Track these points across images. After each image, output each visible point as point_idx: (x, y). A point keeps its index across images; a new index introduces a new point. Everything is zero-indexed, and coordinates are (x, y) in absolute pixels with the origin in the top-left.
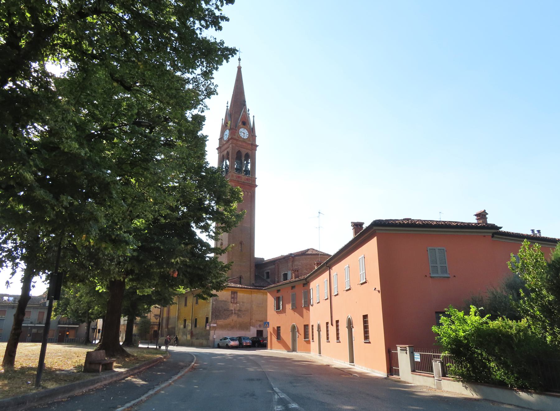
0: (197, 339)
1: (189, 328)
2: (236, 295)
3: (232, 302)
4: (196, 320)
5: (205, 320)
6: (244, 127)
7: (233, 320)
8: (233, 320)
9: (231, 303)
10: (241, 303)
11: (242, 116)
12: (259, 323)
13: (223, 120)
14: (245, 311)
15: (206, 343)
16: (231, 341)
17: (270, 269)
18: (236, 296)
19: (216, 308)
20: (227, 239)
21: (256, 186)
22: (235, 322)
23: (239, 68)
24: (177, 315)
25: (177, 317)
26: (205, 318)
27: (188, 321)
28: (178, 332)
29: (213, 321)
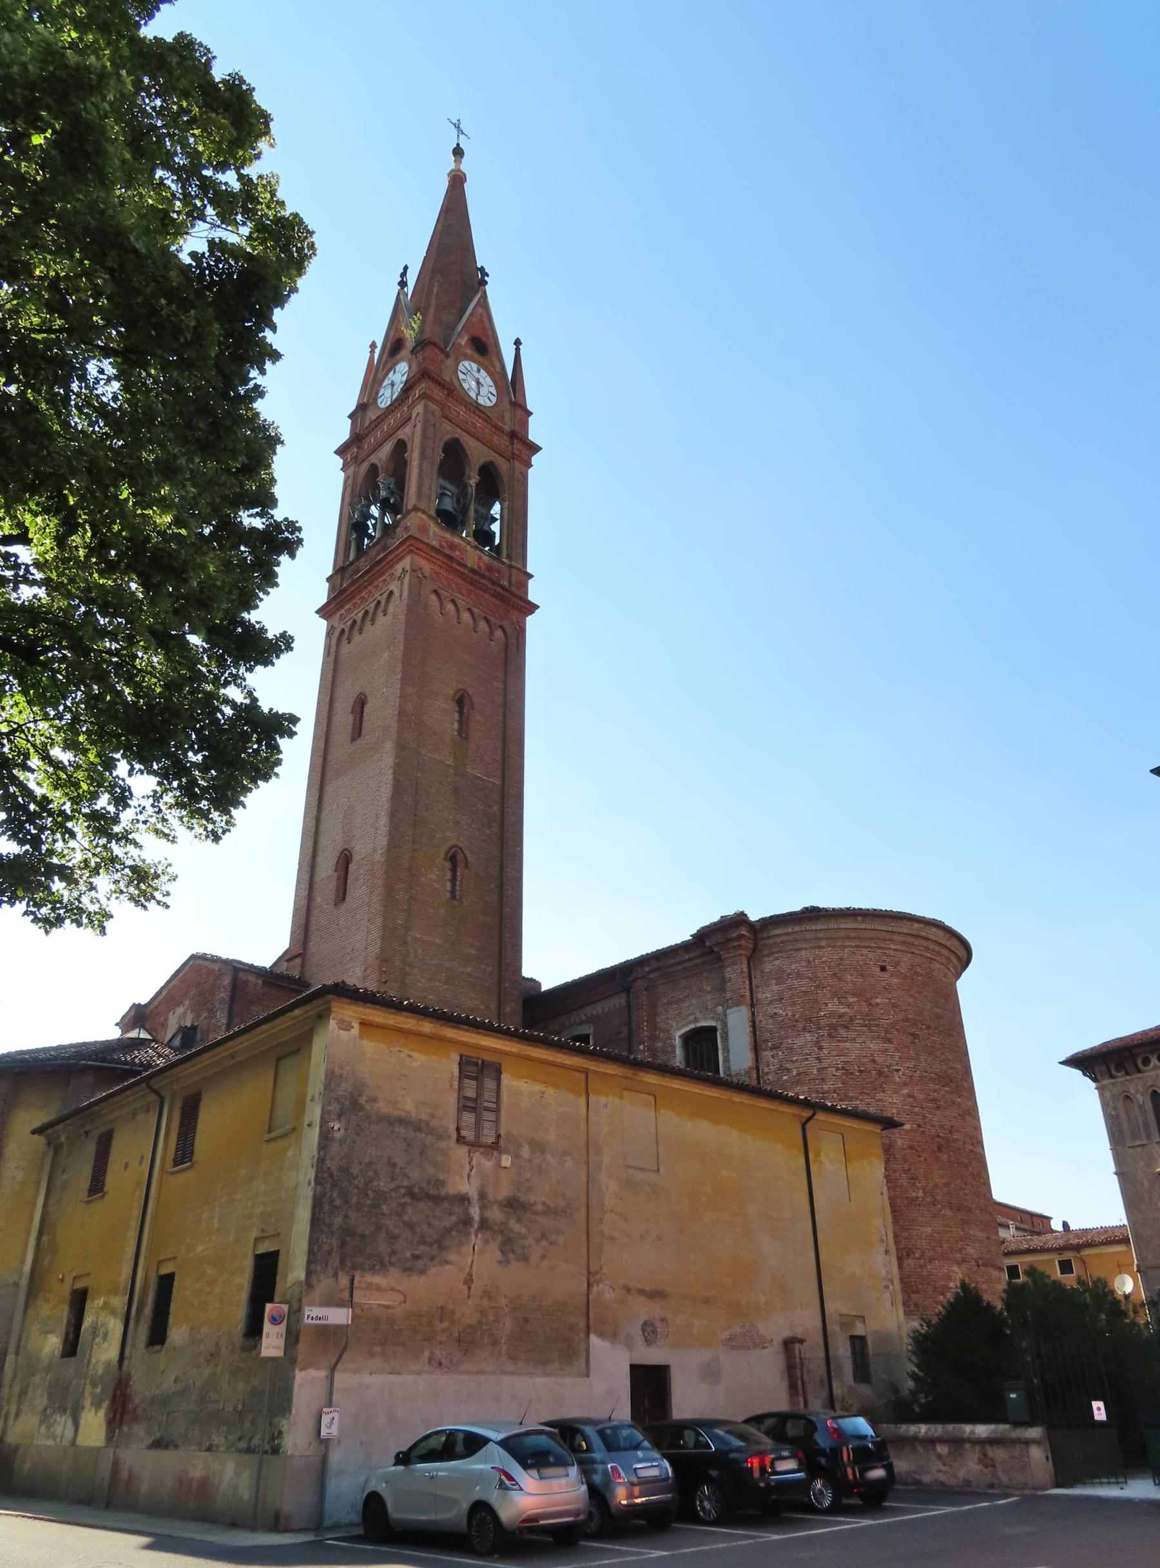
0: (157, 1444)
1: (106, 1352)
2: (489, 1084)
3: (468, 1134)
4: (166, 1284)
5: (243, 1281)
6: (480, 359)
7: (469, 1280)
8: (469, 1280)
9: (460, 1140)
10: (526, 1152)
11: (471, 314)
12: (644, 1310)
13: (373, 346)
14: (548, 1211)
15: (245, 1493)
16: (515, 1469)
17: (590, 1020)
18: (489, 1095)
19: (345, 1170)
20: (384, 821)
21: (532, 608)
22: (486, 1294)
23: (457, 181)
24: (27, 1267)
25: (24, 1282)
26: (249, 1263)
27: (101, 1302)
28: (17, 1389)
29: (325, 1283)
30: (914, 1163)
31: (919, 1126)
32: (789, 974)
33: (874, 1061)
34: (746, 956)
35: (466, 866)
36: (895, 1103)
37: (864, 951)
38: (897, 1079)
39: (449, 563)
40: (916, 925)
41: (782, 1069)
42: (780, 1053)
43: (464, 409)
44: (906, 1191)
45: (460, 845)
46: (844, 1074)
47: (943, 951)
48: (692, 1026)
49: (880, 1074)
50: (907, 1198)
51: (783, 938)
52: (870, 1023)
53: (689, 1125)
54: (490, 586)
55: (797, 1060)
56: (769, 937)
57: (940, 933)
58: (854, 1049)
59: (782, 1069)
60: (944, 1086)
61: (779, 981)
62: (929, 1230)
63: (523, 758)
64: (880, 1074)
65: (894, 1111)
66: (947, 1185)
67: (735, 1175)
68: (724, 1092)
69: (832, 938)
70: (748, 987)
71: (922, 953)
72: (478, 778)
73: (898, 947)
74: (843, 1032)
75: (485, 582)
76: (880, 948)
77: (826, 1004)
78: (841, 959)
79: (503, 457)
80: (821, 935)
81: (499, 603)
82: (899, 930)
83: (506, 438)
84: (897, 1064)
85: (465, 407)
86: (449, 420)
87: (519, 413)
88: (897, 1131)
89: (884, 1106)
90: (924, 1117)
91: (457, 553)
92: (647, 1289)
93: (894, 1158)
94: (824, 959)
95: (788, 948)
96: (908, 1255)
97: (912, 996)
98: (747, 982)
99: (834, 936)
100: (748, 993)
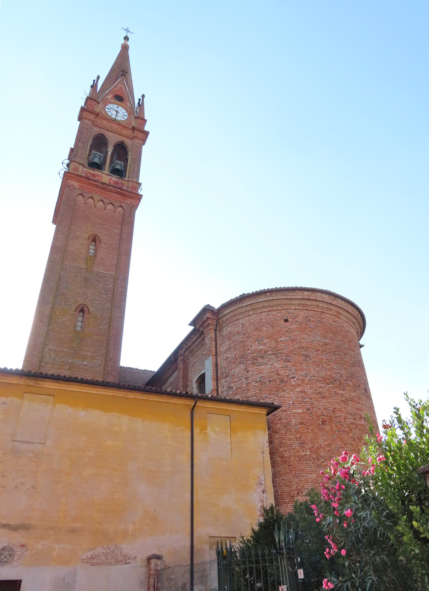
23: (125, 48)
30: (304, 434)
31: (309, 410)
32: (234, 334)
33: (278, 374)
34: (213, 329)
35: (89, 313)
36: (291, 397)
37: (274, 313)
38: (293, 383)
39: (89, 181)
40: (306, 293)
41: (230, 388)
42: (229, 379)
44: (298, 451)
45: (86, 303)
46: (260, 384)
47: (331, 307)
48: (199, 375)
49: (282, 381)
50: (298, 456)
51: (231, 315)
52: (276, 353)
53: (83, 413)
54: (113, 189)
55: (236, 381)
56: (224, 316)
57: (327, 297)
58: (266, 369)
59: (230, 388)
60: (328, 384)
61: (229, 338)
62: (314, 476)
63: (130, 262)
64: (282, 381)
65: (291, 402)
66: (329, 445)
67: (120, 444)
69: (255, 309)
70: (214, 346)
71: (315, 309)
72: (101, 273)
73: (296, 307)
74: (260, 360)
75: (111, 188)
76: (284, 310)
77: (252, 346)
78: (261, 319)
79: (129, 138)
80: (248, 308)
81: (120, 196)
82: (294, 297)
83: (130, 131)
84: (293, 374)
85: (107, 120)
86: (97, 127)
87: (139, 121)
88: (278, 411)
89: (284, 400)
91: (97, 178)
92: (12, 523)
93: (290, 431)
94: (251, 322)
95: (234, 320)
96: (298, 494)
97: (306, 333)
98: (214, 343)
99: (255, 308)
100: (214, 349)
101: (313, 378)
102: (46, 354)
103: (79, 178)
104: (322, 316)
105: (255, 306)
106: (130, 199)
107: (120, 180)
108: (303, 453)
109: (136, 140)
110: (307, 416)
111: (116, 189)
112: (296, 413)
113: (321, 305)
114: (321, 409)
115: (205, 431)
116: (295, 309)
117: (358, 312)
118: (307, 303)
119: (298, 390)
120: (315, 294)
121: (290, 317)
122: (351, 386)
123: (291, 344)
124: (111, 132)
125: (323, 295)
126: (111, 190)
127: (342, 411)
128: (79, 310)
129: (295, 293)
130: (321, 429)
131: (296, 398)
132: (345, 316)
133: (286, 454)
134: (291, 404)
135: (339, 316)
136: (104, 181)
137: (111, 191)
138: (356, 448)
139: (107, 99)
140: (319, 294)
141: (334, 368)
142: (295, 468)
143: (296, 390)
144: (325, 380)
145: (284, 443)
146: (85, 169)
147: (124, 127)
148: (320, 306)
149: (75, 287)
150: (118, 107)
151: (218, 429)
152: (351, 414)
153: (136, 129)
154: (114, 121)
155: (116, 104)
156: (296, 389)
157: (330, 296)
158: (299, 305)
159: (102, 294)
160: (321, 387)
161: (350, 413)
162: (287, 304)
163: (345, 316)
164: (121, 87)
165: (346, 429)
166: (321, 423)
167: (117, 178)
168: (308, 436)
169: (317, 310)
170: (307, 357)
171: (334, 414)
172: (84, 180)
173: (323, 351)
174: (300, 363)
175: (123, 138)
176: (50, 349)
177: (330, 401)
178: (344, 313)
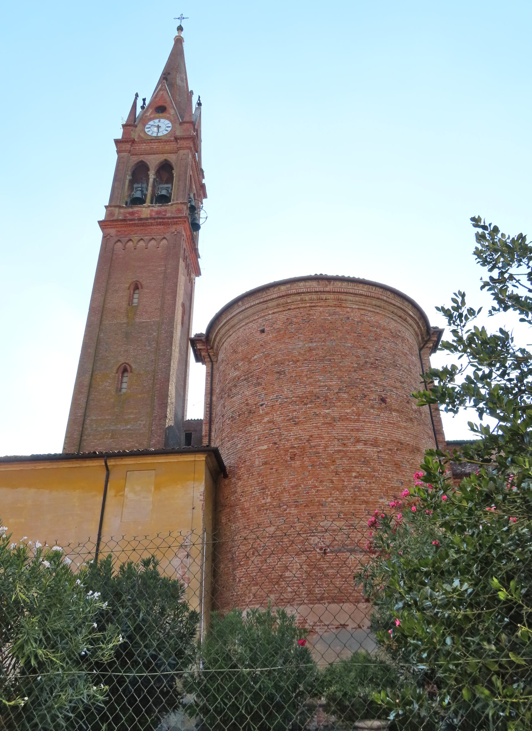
23: (179, 41)
31: (275, 443)
33: (247, 404)
35: (131, 372)
39: (125, 223)
40: (283, 288)
43: (145, 144)
44: (258, 500)
47: (324, 296)
50: (257, 506)
52: (248, 376)
57: (314, 284)
65: (256, 437)
67: (23, 520)
68: (26, 465)
71: (300, 305)
72: (143, 322)
73: (275, 310)
75: (150, 221)
81: (163, 227)
82: (269, 298)
83: (173, 143)
85: (145, 143)
86: (135, 155)
90: (280, 435)
101: (285, 400)
102: (88, 426)
103: (115, 224)
104: (311, 312)
105: (232, 323)
106: (175, 226)
107: (163, 208)
108: (263, 501)
109: (181, 152)
110: (273, 452)
111: (156, 220)
112: (261, 450)
113: (307, 297)
114: (291, 440)
115: (121, 493)
116: (274, 313)
117: (381, 290)
118: (286, 300)
119: (266, 420)
120: (296, 285)
121: (267, 325)
122: (346, 399)
123: (264, 361)
124: (151, 154)
125: (307, 284)
126: (151, 223)
127: (323, 438)
128: (122, 370)
129: (269, 292)
130: (288, 466)
131: (263, 431)
132: (356, 302)
133: (246, 505)
134: (257, 440)
135: (344, 305)
136: (143, 216)
137: (152, 224)
138: (339, 484)
139: (146, 116)
140: (302, 284)
141: (319, 381)
142: (253, 521)
143: (263, 421)
144: (302, 400)
145: (246, 492)
146: (122, 211)
147: (165, 142)
148: (307, 299)
149: (115, 347)
150: (159, 121)
151: (138, 488)
152: (338, 440)
153: (179, 139)
154: (157, 140)
155: (156, 118)
156: (263, 419)
157: (319, 282)
158: (278, 305)
159: (145, 346)
160: (295, 411)
161: (336, 438)
162: (263, 310)
163: (356, 302)
164: (163, 94)
165: (326, 461)
166: (289, 458)
167: (159, 206)
168: (271, 478)
169: (304, 305)
170: (281, 374)
171: (309, 443)
172: (120, 223)
173: (306, 360)
174: (272, 384)
175: (166, 155)
176: (92, 420)
177: (306, 426)
178: (350, 298)
